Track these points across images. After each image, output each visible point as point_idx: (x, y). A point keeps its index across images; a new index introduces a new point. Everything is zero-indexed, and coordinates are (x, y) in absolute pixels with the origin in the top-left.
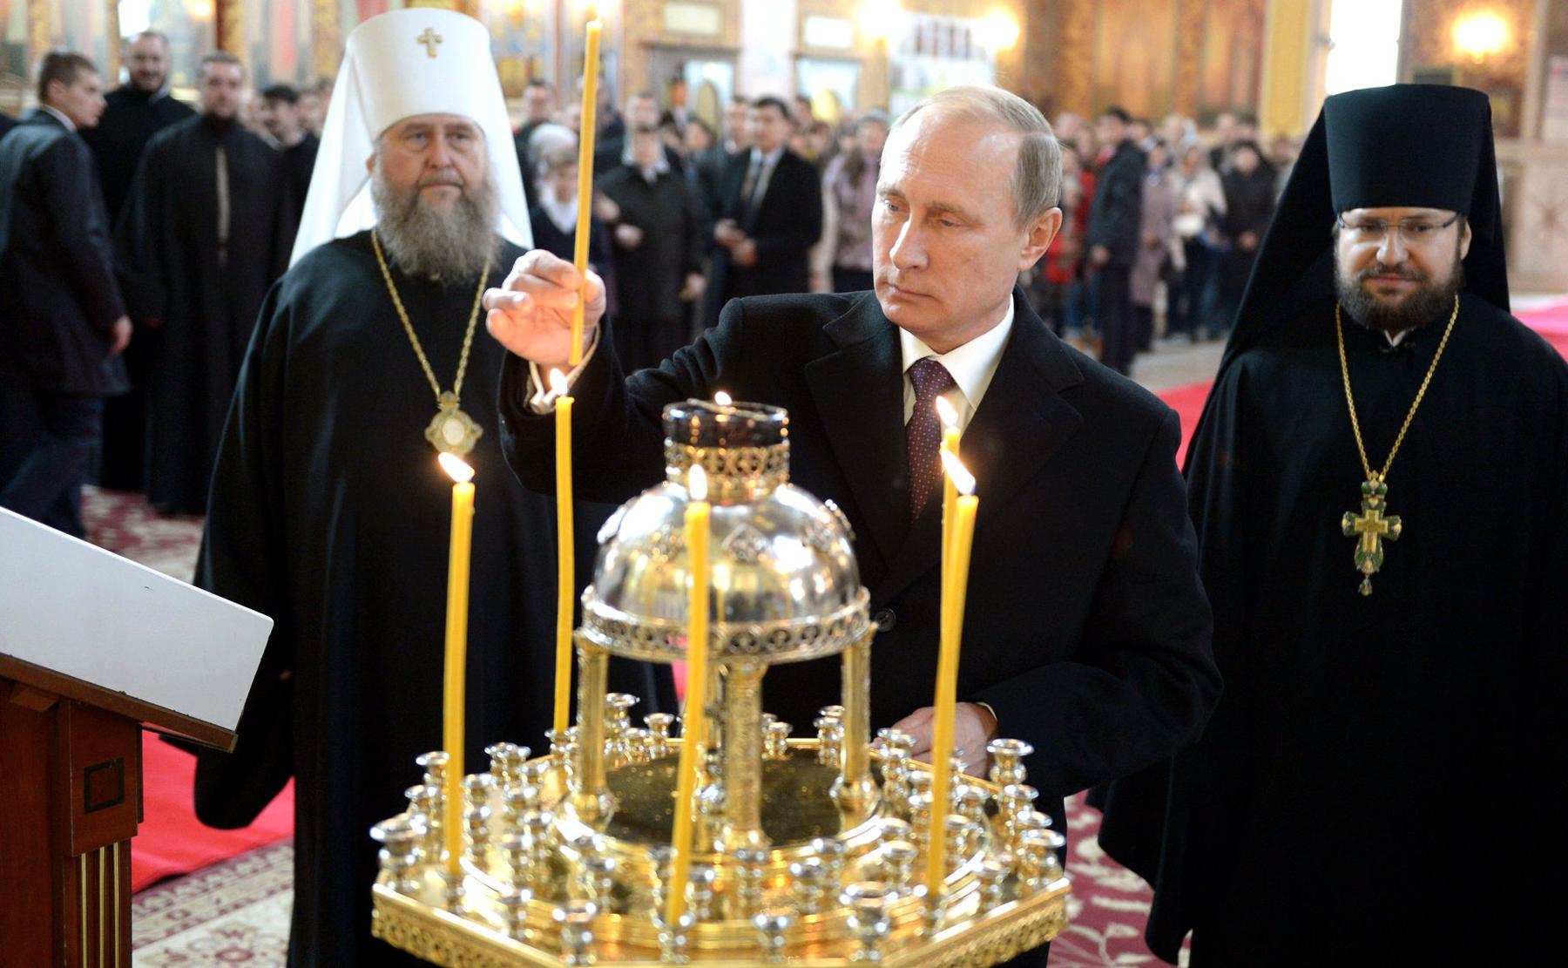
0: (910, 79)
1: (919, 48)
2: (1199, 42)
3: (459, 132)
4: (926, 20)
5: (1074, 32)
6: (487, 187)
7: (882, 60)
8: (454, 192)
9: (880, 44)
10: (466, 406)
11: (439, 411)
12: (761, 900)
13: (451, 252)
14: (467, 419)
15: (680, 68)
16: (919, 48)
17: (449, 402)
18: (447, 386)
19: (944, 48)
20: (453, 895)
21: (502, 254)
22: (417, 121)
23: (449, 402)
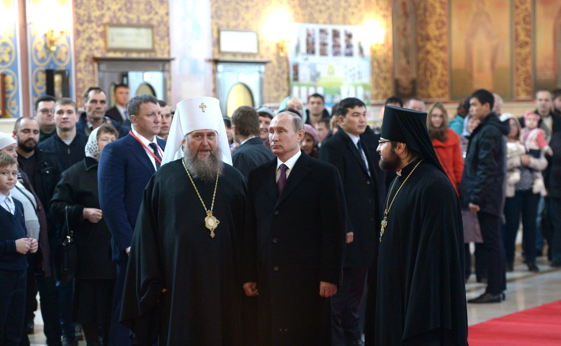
0: (304, 73)
1: (311, 51)
2: (531, 33)
3: (211, 134)
4: (315, 28)
5: (432, 30)
6: (218, 150)
7: (282, 60)
8: (209, 153)
9: (280, 48)
10: (214, 215)
11: (207, 215)
12: (450, 128)
13: (208, 172)
14: (215, 218)
15: (125, 75)
16: (311, 51)
17: (209, 213)
18: (209, 208)
19: (329, 48)
20: (472, 116)
21: (386, 150)
22: (199, 132)
23: (209, 213)
